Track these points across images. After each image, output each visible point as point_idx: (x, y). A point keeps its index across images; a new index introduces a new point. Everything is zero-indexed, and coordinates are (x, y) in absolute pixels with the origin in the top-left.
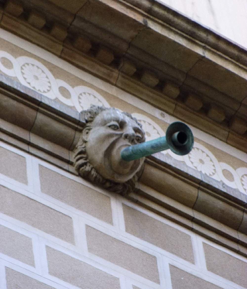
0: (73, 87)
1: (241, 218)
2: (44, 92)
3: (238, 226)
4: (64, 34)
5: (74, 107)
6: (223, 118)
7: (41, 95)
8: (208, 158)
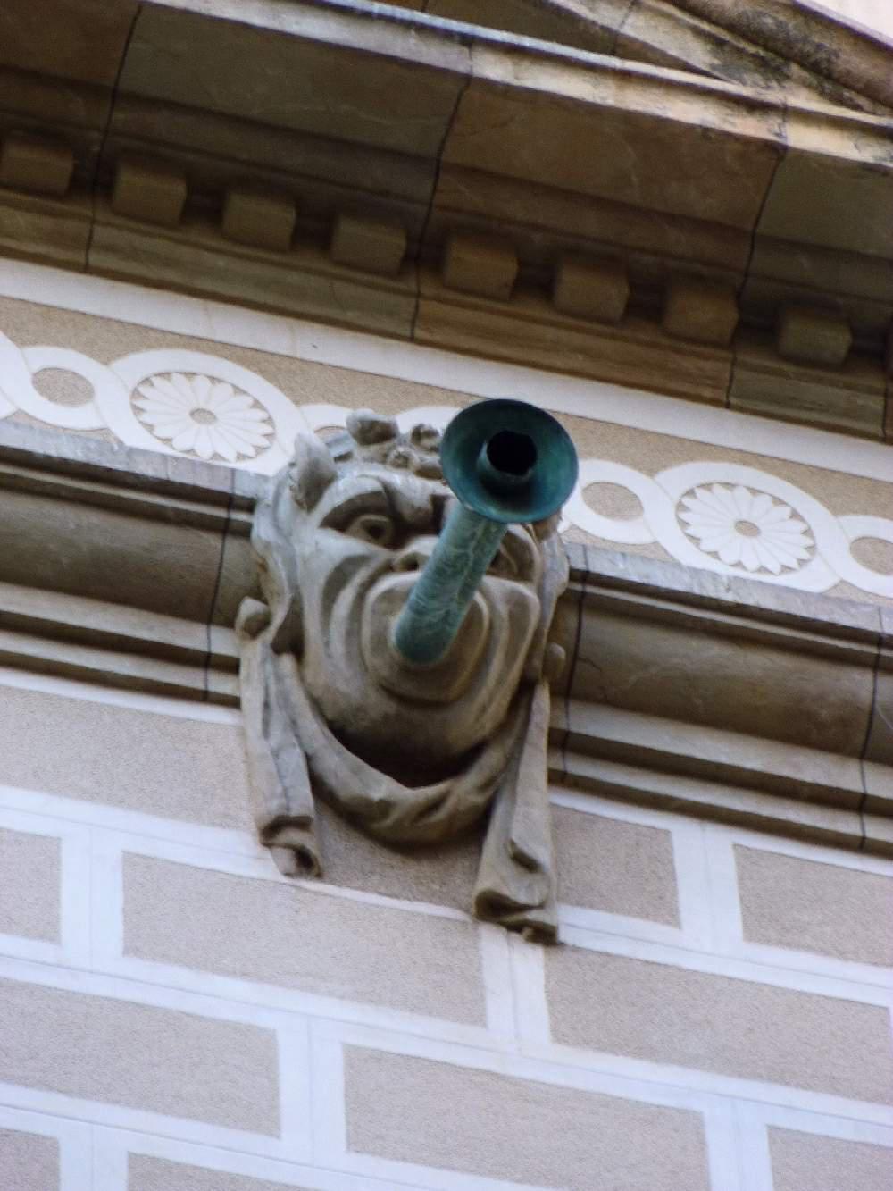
0: (651, 472)
1: (214, 574)
2: (786, 569)
3: (859, 737)
4: (280, 218)
5: (19, 412)
6: (731, 316)
7: (233, 471)
8: (219, 387)
